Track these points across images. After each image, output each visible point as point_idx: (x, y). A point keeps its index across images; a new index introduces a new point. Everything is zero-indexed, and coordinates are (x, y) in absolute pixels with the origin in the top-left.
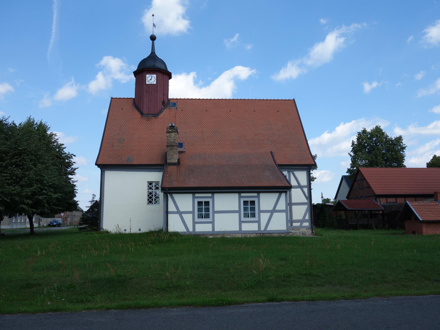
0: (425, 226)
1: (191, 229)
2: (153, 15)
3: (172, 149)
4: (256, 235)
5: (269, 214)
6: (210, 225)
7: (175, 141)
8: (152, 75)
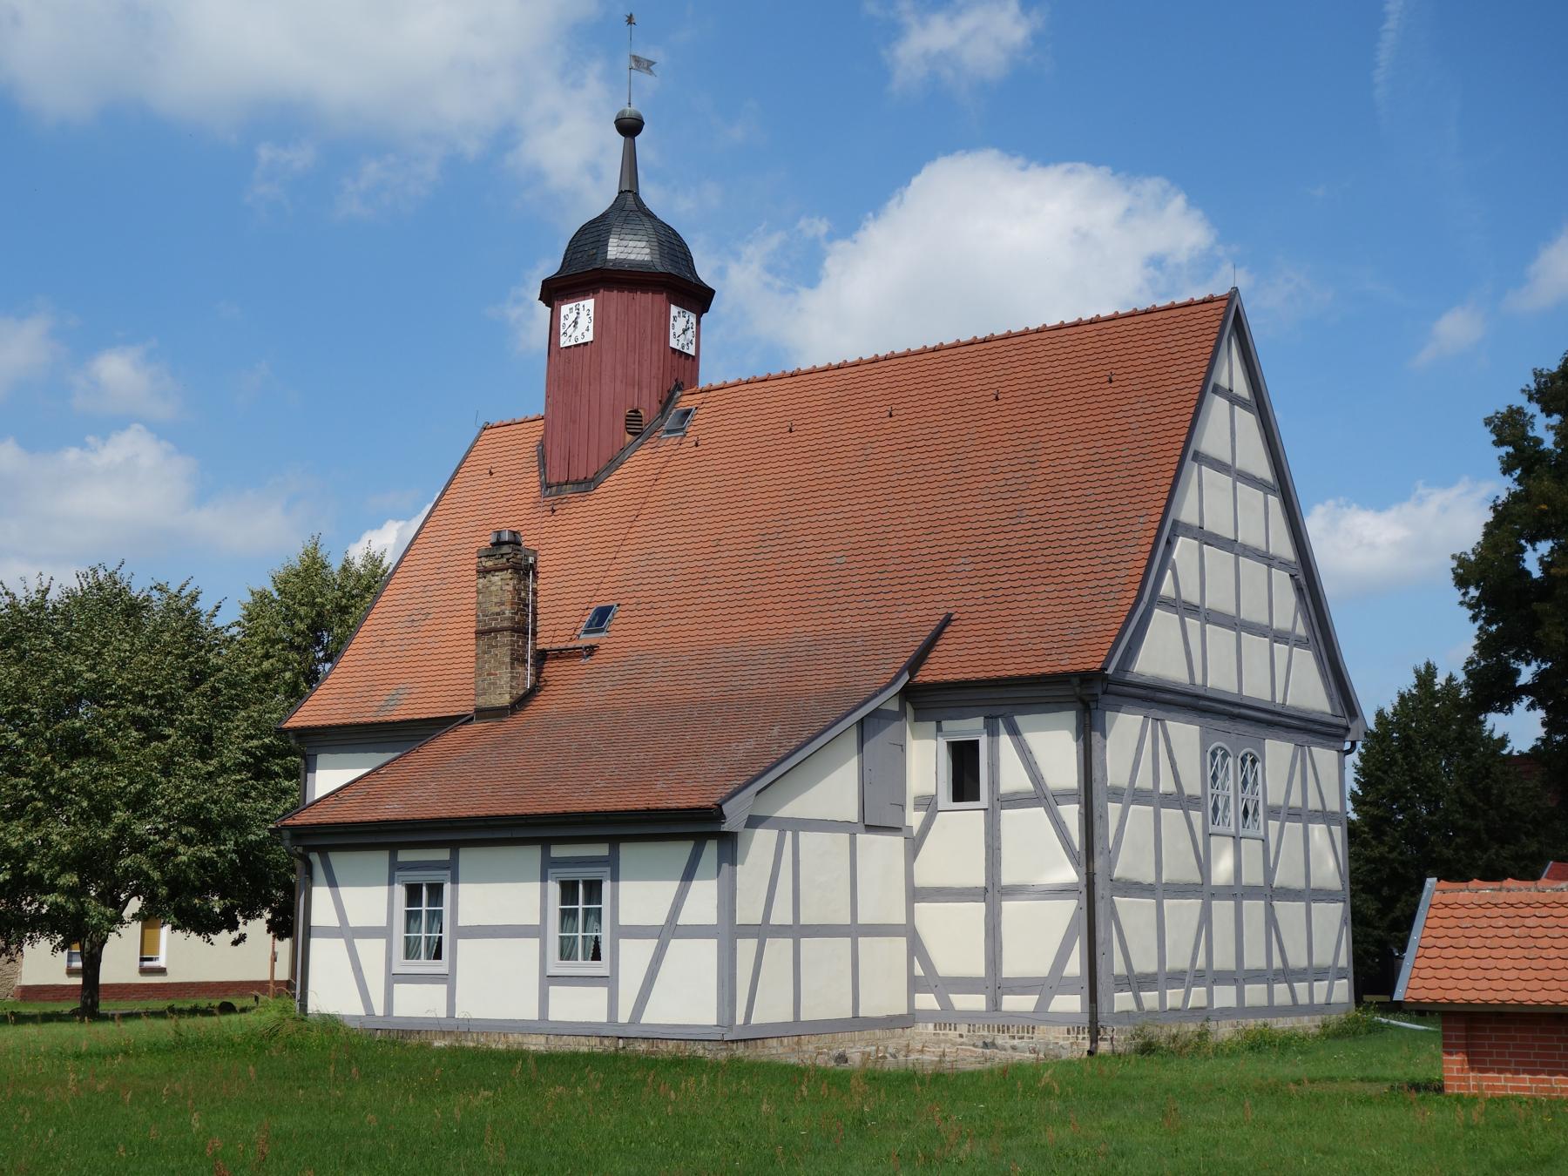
0: (1457, 1038)
1: (379, 1010)
2: (630, 20)
3: (493, 647)
4: (601, 1043)
5: (650, 945)
6: (441, 990)
7: (503, 607)
8: (582, 303)
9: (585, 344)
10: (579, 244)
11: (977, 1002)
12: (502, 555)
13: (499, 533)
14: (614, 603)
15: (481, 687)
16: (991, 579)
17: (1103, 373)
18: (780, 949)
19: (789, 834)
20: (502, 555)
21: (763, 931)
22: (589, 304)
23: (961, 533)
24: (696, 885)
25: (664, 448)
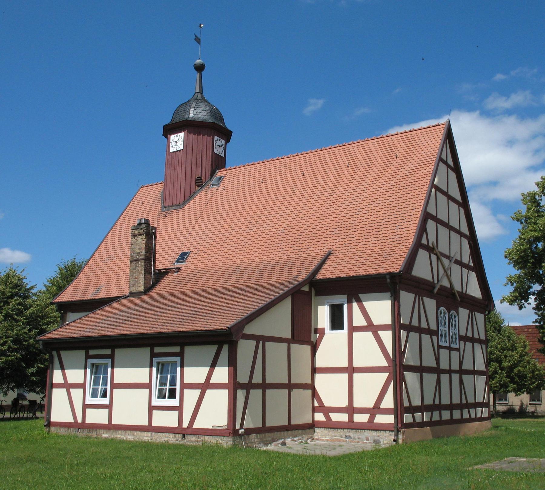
5: (197, 392)
9: (180, 150)
10: (178, 111)
11: (343, 418)
12: (141, 229)
13: (140, 219)
14: (189, 251)
15: (132, 284)
16: (348, 237)
17: (393, 155)
18: (256, 394)
19: (261, 343)
20: (141, 229)
21: (249, 387)
22: (182, 134)
23: (334, 219)
24: (217, 369)
25: (211, 191)
